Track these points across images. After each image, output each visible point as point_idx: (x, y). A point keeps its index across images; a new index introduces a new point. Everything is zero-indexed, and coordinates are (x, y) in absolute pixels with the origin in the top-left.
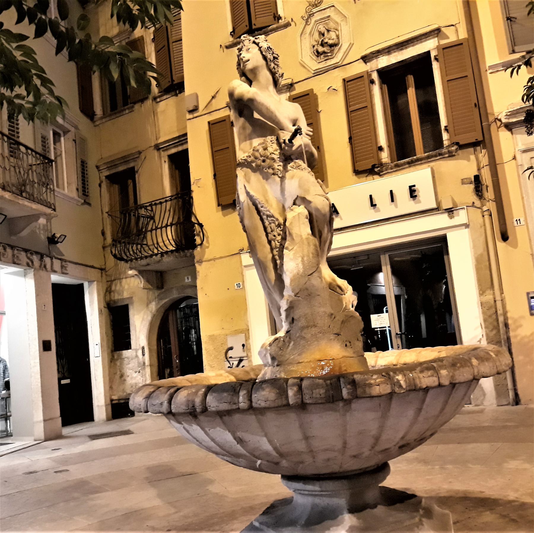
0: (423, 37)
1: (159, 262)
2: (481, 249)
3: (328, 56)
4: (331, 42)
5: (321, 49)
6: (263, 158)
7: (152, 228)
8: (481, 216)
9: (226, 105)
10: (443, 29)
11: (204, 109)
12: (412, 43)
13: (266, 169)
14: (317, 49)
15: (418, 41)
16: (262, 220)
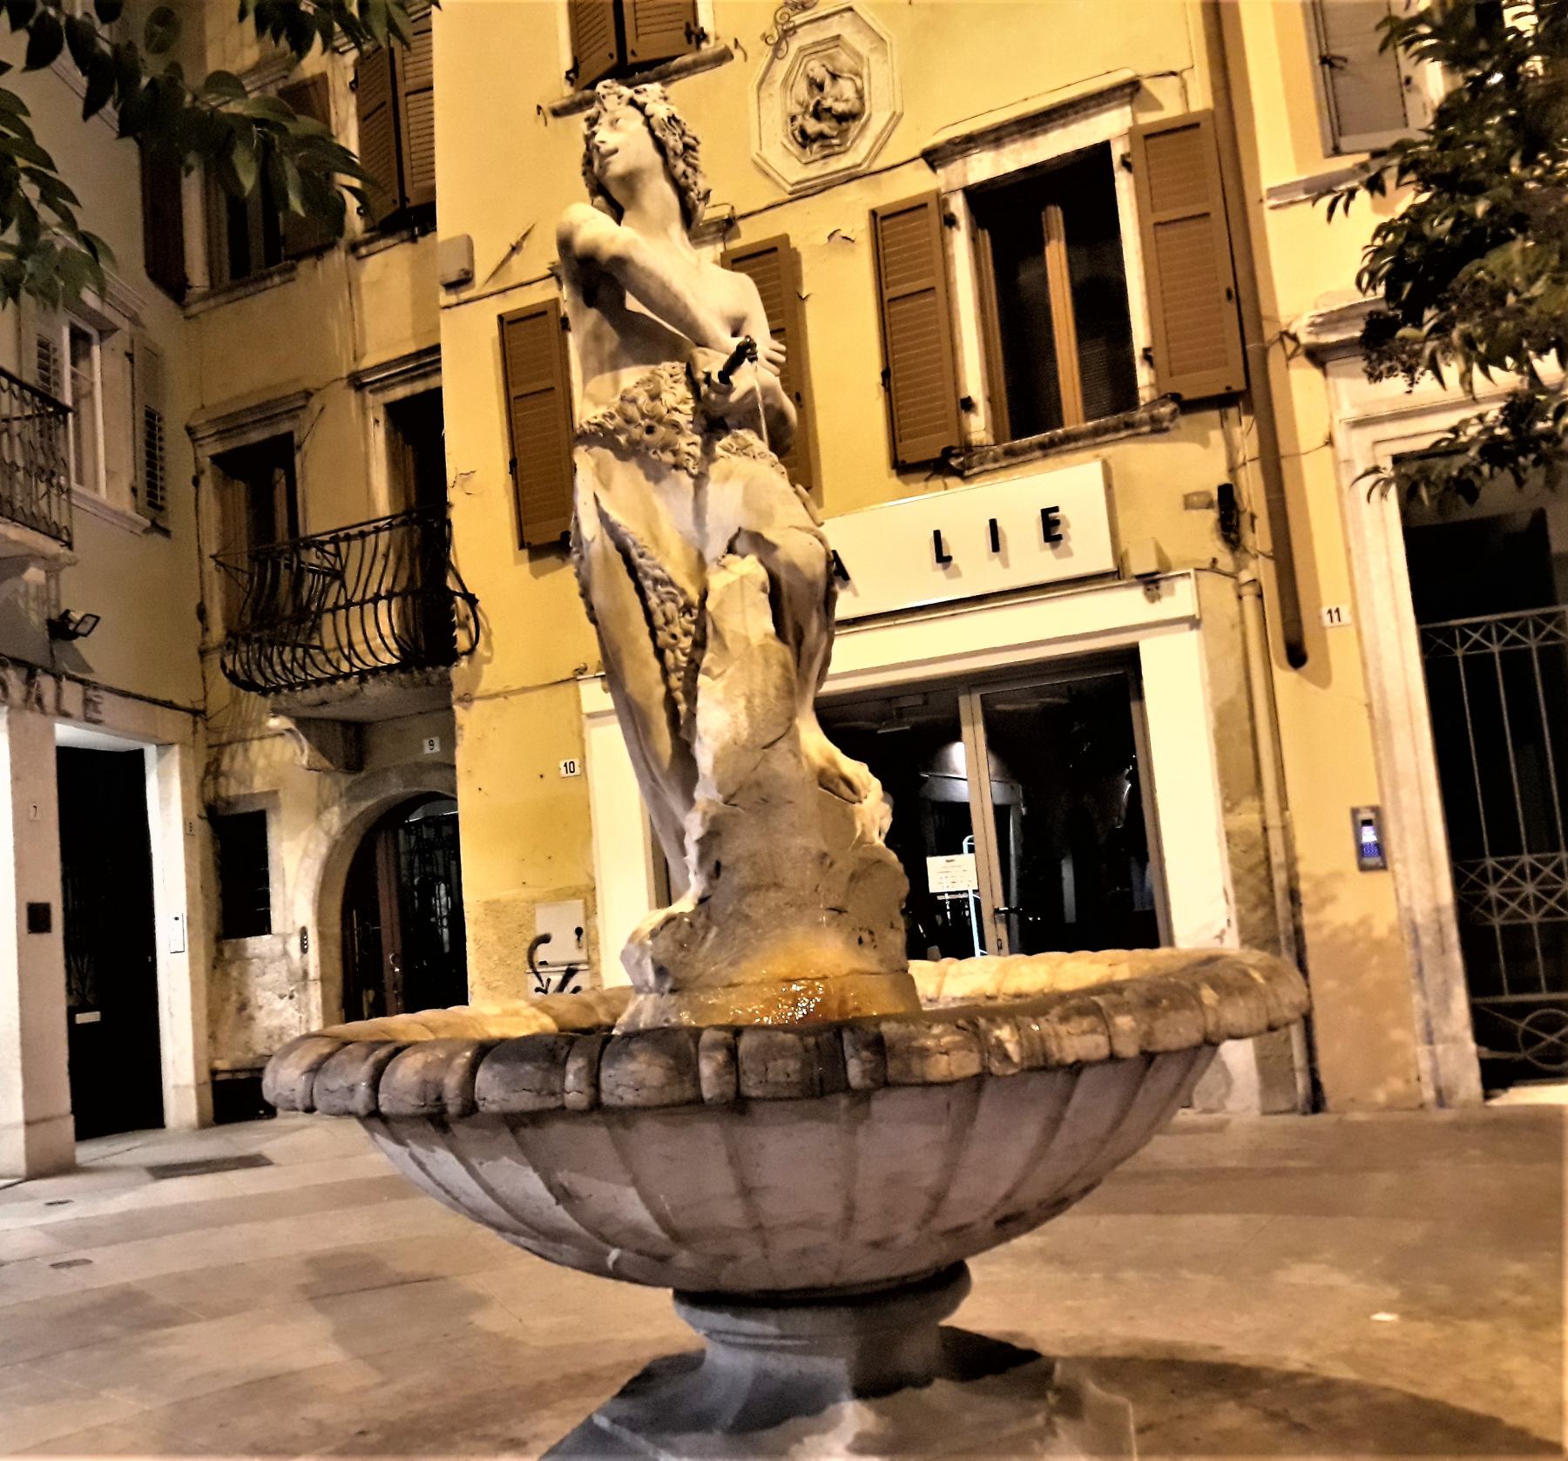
0: (1093, 102)
3: (832, 146)
4: (840, 107)
5: (812, 126)
6: (647, 421)
9: (549, 272)
12: (1062, 117)
15: (1077, 113)
16: (640, 590)
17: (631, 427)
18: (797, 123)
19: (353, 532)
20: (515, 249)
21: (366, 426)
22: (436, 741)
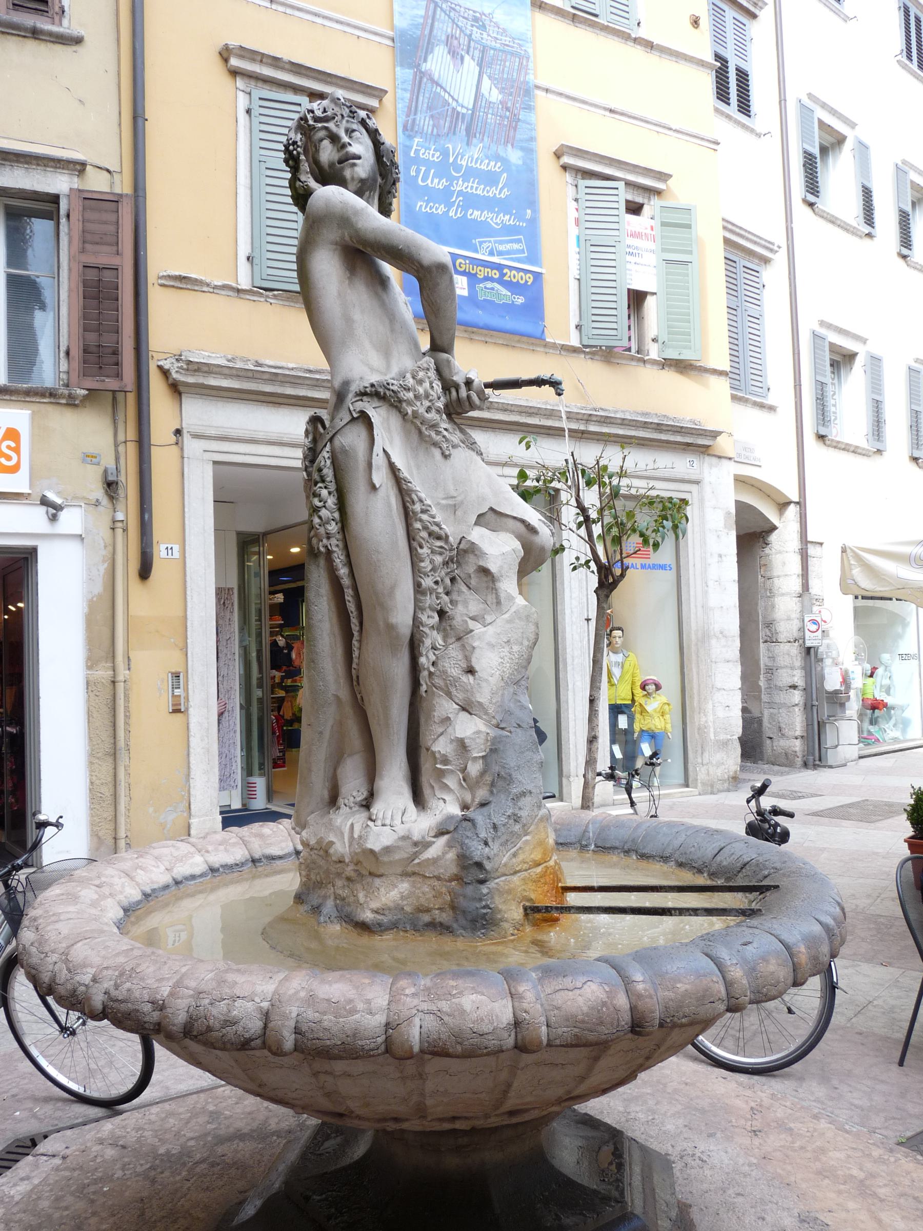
0: (52, 164)
2: (98, 588)
8: (109, 524)
10: (88, 168)
12: (27, 163)
15: (38, 165)
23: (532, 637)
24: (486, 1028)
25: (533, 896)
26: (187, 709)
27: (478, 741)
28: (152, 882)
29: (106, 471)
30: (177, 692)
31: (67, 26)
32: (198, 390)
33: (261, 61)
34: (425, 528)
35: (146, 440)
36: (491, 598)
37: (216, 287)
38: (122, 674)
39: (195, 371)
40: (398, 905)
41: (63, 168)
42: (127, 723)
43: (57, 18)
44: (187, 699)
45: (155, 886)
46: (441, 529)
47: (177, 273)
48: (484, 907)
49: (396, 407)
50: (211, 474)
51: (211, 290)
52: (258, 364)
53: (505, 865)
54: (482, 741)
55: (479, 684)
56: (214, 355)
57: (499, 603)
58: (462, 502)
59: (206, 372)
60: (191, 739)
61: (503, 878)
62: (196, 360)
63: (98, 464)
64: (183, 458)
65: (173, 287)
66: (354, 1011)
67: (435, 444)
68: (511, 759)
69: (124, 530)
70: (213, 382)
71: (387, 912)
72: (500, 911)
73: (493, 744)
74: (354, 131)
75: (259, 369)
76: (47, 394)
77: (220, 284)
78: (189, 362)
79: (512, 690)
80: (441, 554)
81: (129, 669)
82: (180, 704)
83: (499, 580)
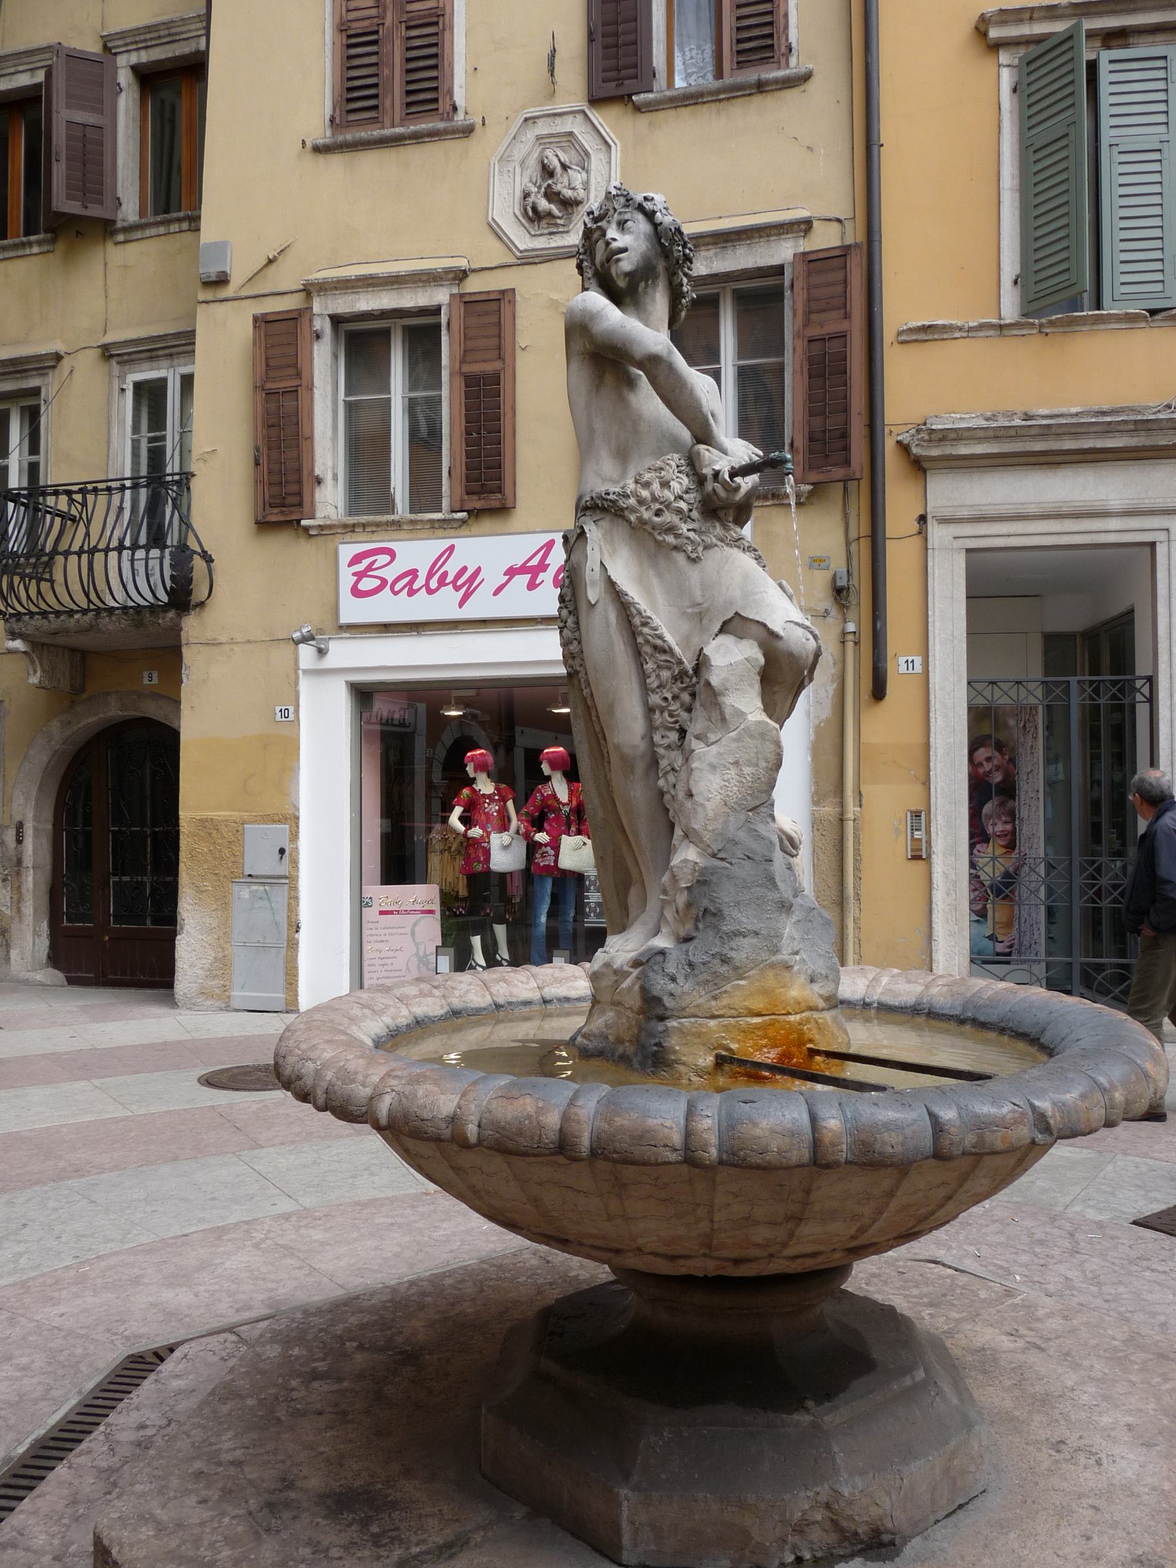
0: (775, 231)
1: (91, 628)
3: (557, 225)
4: (568, 193)
5: (543, 204)
6: (658, 506)
7: (82, 547)
9: (302, 287)
10: (816, 224)
11: (243, 285)
12: (749, 238)
13: (659, 534)
14: (533, 203)
15: (761, 237)
16: (638, 654)
17: (643, 509)
18: (530, 200)
19: (101, 486)
20: (270, 262)
21: (110, 393)
22: (155, 675)
23: (772, 757)
24: (426, 1115)
25: (734, 1046)
26: (929, 856)
27: (685, 870)
28: (511, 996)
29: (834, 576)
30: (917, 835)
31: (795, 64)
32: (945, 464)
33: (1031, 18)
34: (647, 642)
35: (880, 534)
36: (715, 715)
37: (970, 329)
38: (851, 809)
39: (940, 440)
40: (603, 1032)
41: (787, 233)
42: (857, 869)
43: (783, 61)
44: (929, 843)
45: (513, 1000)
46: (664, 641)
47: (919, 324)
48: (656, 1045)
49: (620, 516)
50: (964, 565)
51: (965, 334)
52: (1028, 417)
53: (697, 1006)
54: (689, 871)
55: (694, 809)
56: (967, 416)
57: (723, 719)
58: (708, 609)
59: (954, 440)
60: (934, 892)
61: (693, 1020)
62: (940, 427)
63: (828, 568)
64: (926, 549)
65: (916, 341)
66: (353, 1081)
67: (676, 548)
68: (725, 894)
69: (856, 643)
70: (963, 450)
71: (592, 1038)
72: (675, 1052)
73: (701, 874)
74: (626, 221)
75: (1029, 423)
76: (770, 496)
77: (976, 324)
78: (932, 431)
79: (743, 817)
80: (669, 668)
81: (860, 806)
82: (921, 850)
83: (722, 694)
